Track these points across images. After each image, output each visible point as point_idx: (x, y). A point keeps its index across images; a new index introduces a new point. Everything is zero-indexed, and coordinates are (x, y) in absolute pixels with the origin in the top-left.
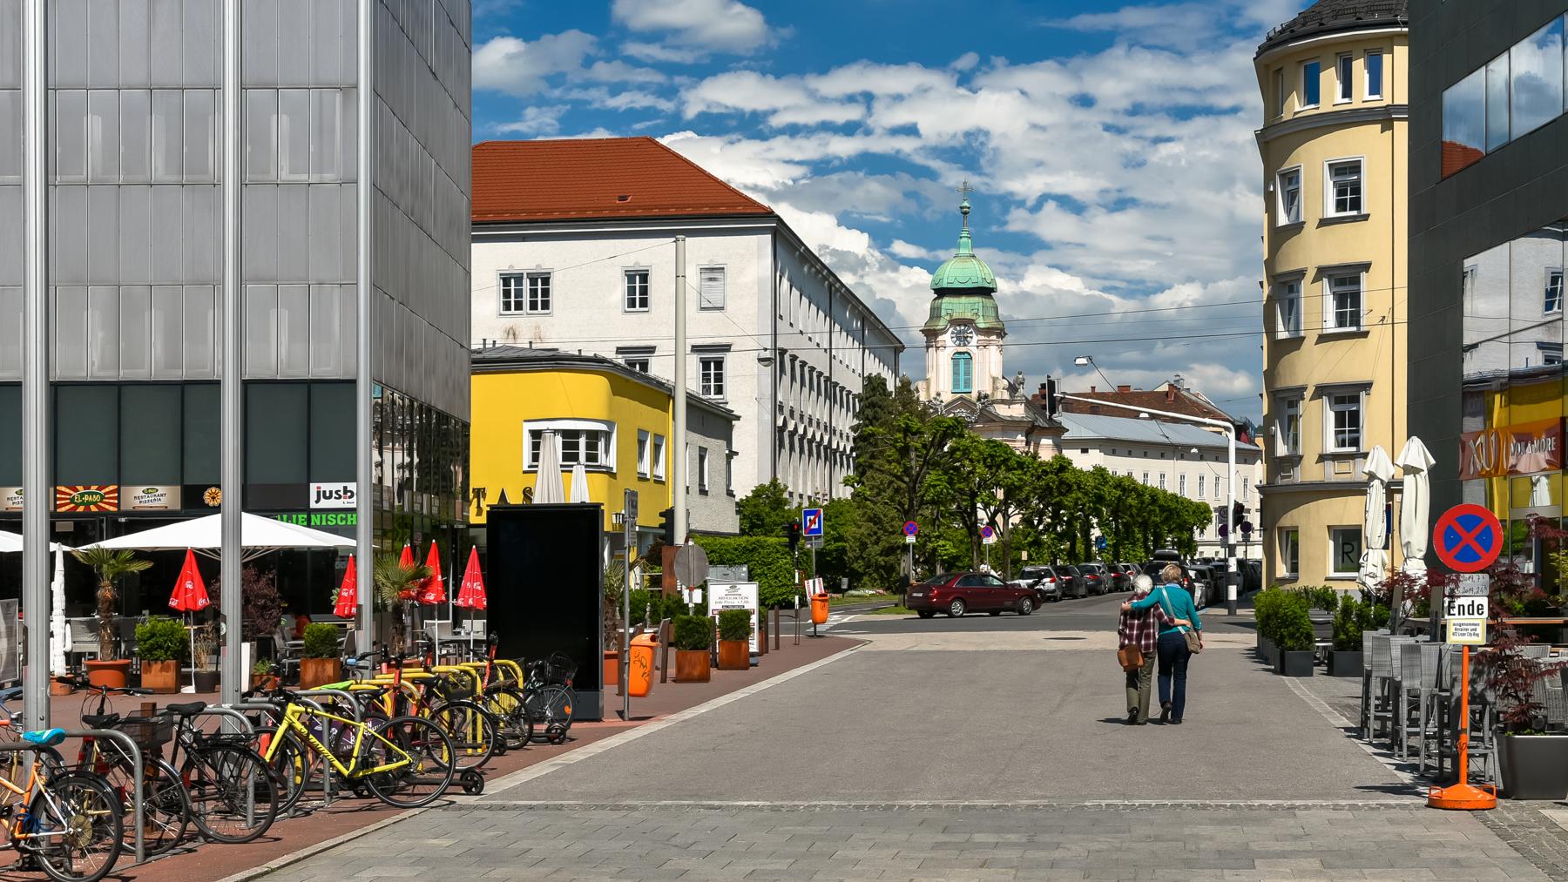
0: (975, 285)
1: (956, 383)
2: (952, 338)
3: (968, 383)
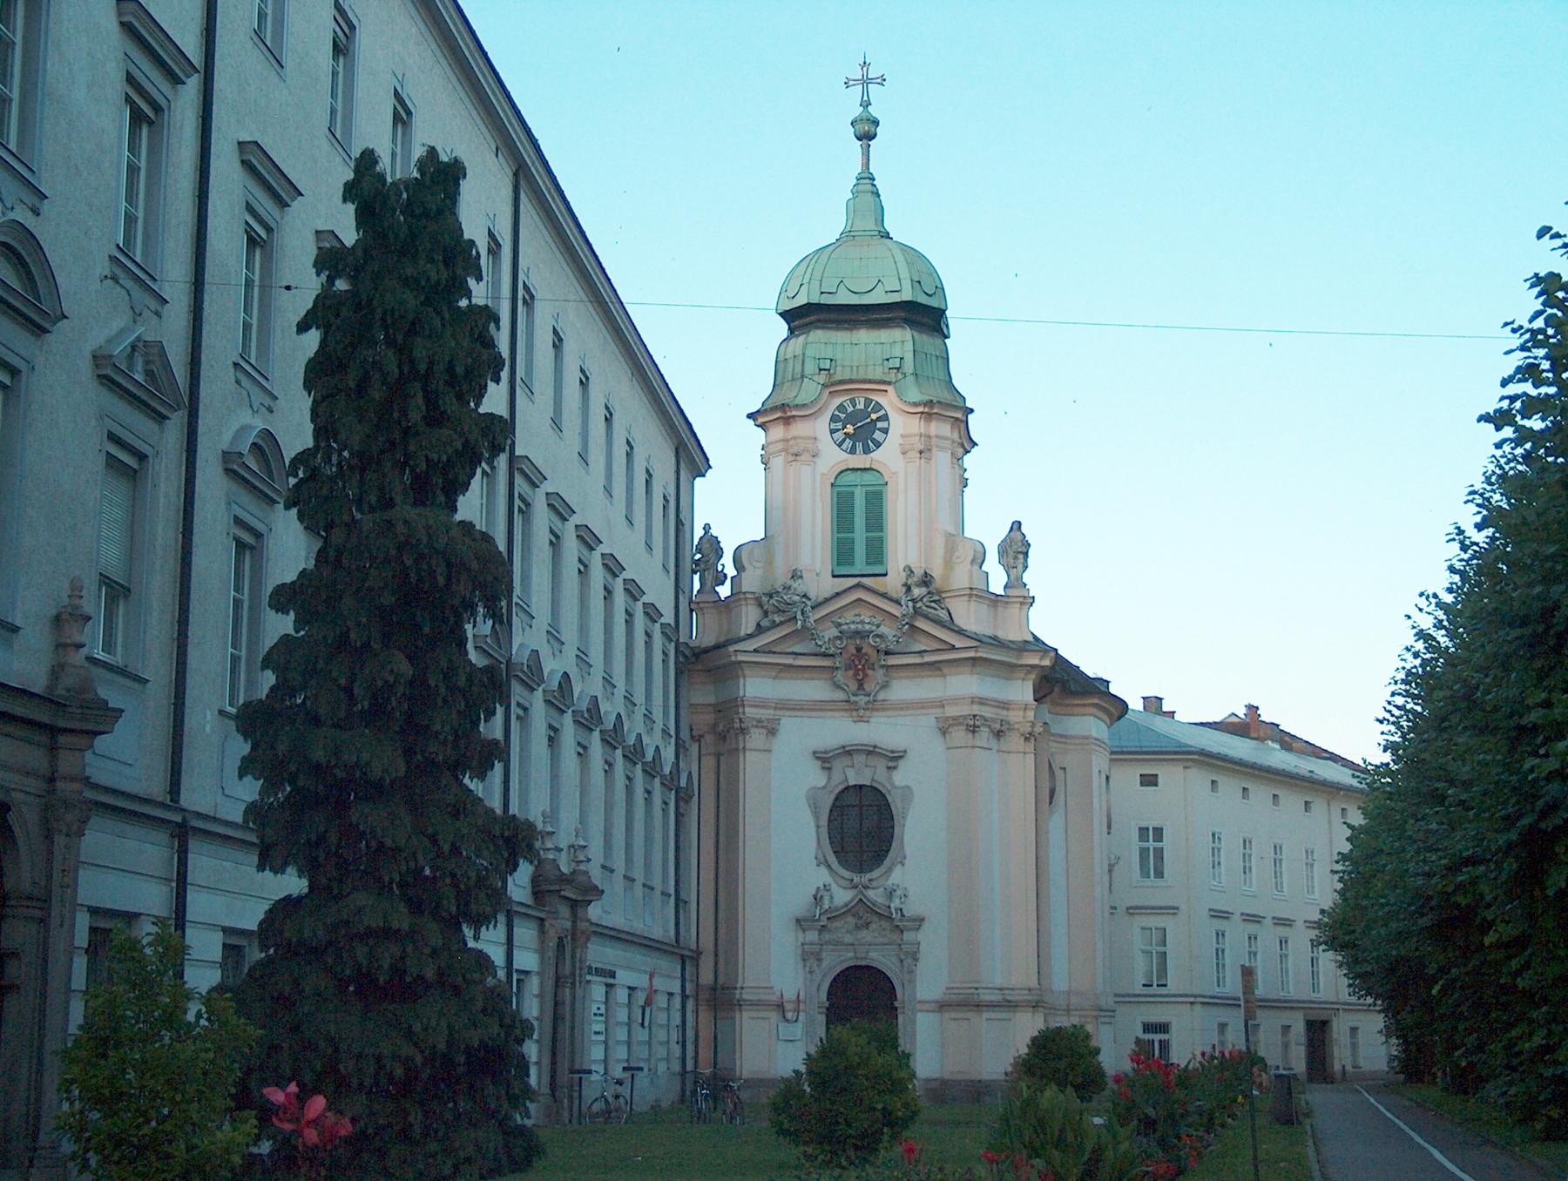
1: (843, 553)
2: (832, 432)
3: (876, 551)
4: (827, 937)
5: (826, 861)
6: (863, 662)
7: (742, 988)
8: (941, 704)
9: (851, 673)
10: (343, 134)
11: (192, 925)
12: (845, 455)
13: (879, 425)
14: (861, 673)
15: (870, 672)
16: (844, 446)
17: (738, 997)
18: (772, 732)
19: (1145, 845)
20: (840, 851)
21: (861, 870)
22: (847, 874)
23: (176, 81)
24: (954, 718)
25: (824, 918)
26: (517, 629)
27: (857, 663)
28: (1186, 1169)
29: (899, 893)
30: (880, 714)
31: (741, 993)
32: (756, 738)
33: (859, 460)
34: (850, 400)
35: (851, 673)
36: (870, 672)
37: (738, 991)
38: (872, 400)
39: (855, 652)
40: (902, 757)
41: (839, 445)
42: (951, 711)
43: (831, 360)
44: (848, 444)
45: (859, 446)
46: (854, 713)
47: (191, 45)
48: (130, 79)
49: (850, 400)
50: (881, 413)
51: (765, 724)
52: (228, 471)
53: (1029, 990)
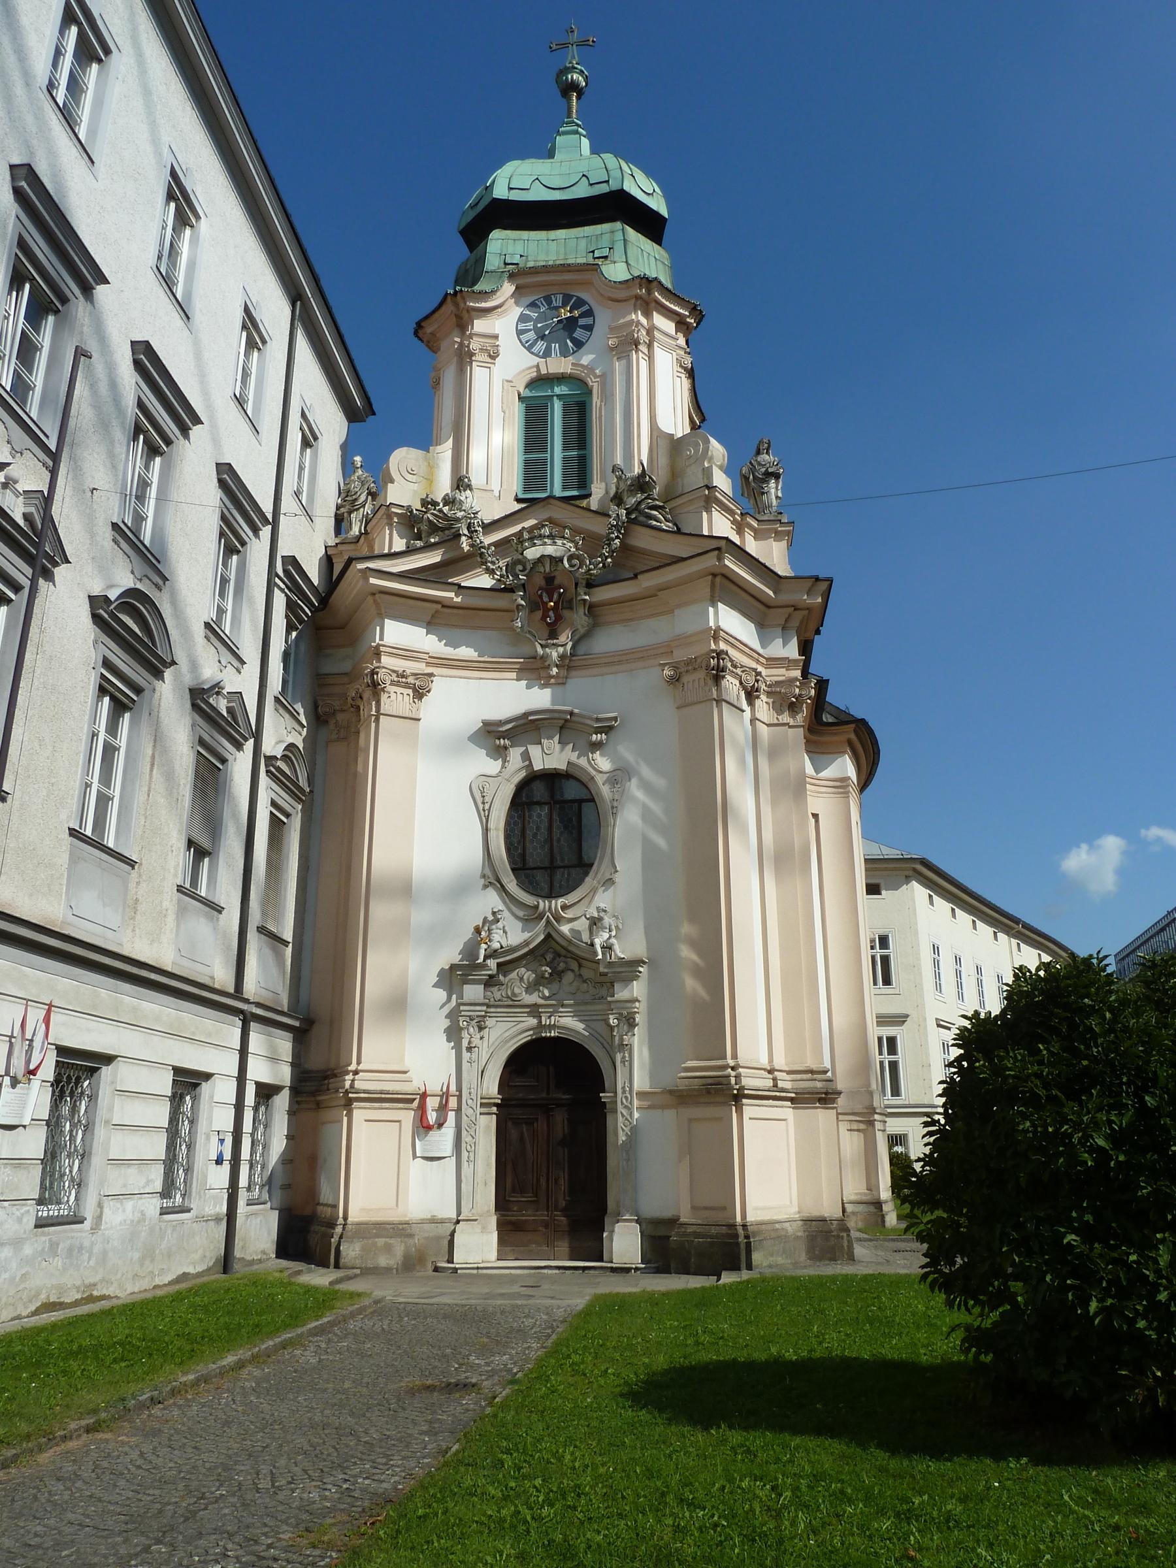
0: (604, 189)
1: (534, 473)
2: (520, 333)
4: (497, 993)
5: (499, 881)
6: (555, 597)
7: (356, 1073)
8: (667, 649)
9: (539, 614)
10: (307, 501)
11: (56, 1009)
12: (536, 360)
13: (582, 322)
14: (551, 613)
15: (566, 613)
16: (535, 349)
17: (347, 1084)
18: (419, 694)
19: (893, 1058)
20: (520, 867)
21: (551, 895)
22: (529, 900)
23: (256, 530)
24: (689, 662)
25: (492, 963)
26: (497, 829)
27: (545, 599)
28: (920, 1282)
29: (607, 920)
30: (583, 672)
31: (353, 1081)
32: (395, 700)
33: (559, 365)
34: (545, 298)
35: (539, 614)
36: (566, 613)
37: (349, 1077)
38: (573, 296)
39: (543, 583)
40: (611, 728)
41: (529, 349)
42: (681, 655)
43: (521, 256)
44: (541, 346)
45: (555, 347)
46: (543, 674)
47: (267, 508)
48: (223, 518)
49: (545, 298)
50: (586, 308)
51: (411, 680)
52: (96, 618)
53: (812, 1072)
